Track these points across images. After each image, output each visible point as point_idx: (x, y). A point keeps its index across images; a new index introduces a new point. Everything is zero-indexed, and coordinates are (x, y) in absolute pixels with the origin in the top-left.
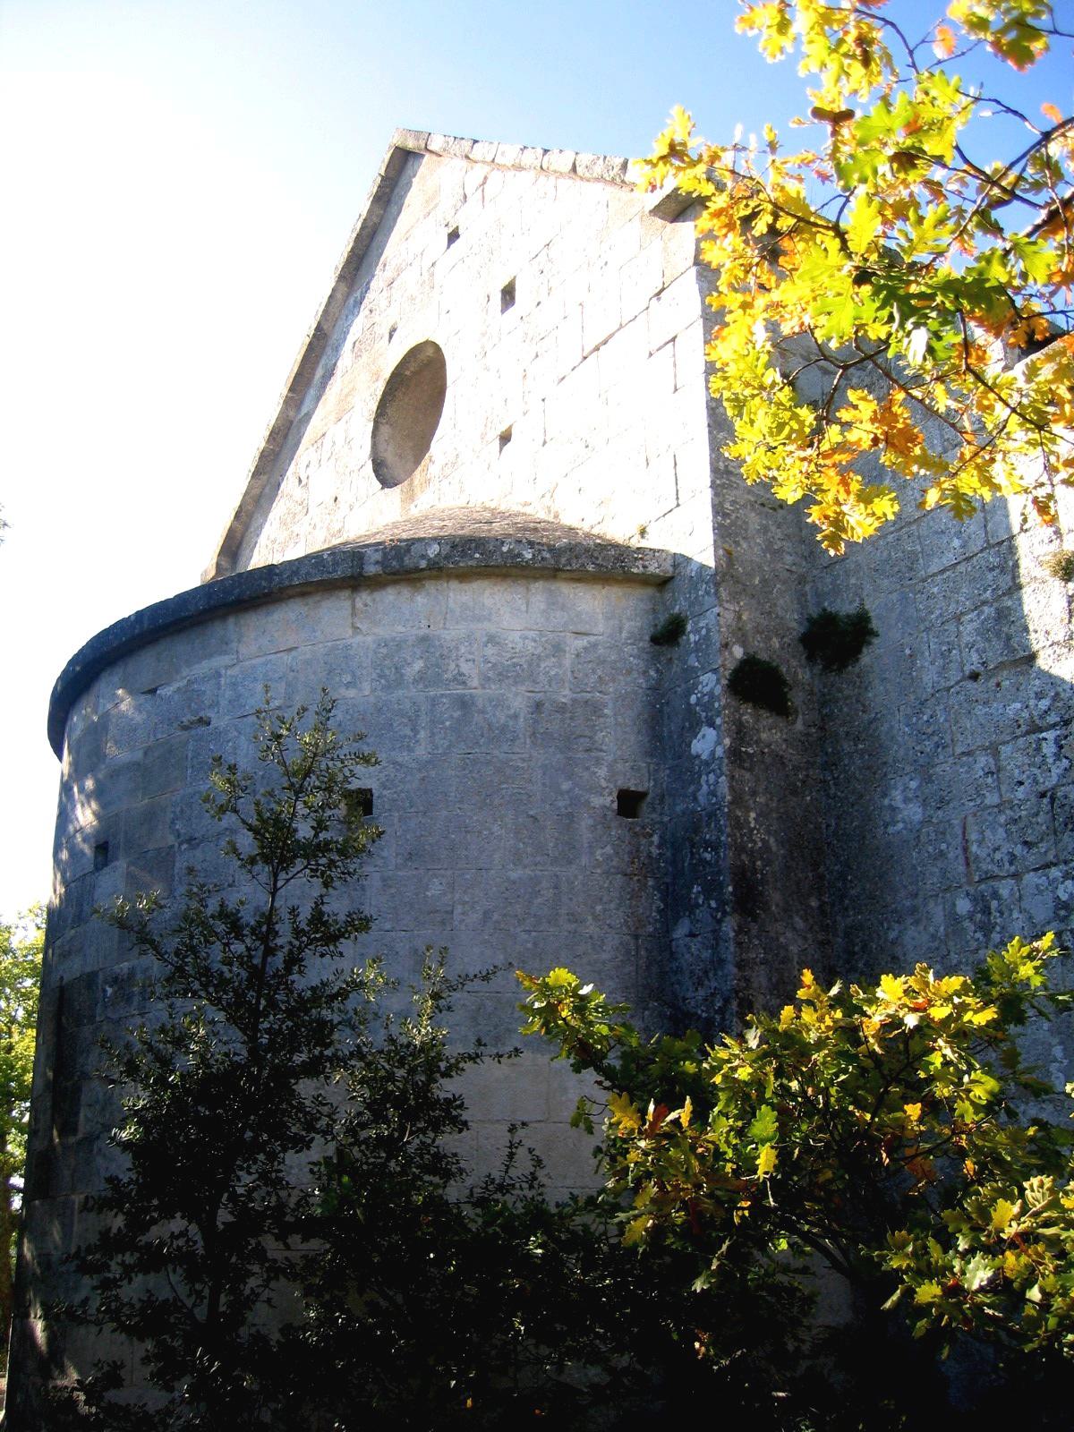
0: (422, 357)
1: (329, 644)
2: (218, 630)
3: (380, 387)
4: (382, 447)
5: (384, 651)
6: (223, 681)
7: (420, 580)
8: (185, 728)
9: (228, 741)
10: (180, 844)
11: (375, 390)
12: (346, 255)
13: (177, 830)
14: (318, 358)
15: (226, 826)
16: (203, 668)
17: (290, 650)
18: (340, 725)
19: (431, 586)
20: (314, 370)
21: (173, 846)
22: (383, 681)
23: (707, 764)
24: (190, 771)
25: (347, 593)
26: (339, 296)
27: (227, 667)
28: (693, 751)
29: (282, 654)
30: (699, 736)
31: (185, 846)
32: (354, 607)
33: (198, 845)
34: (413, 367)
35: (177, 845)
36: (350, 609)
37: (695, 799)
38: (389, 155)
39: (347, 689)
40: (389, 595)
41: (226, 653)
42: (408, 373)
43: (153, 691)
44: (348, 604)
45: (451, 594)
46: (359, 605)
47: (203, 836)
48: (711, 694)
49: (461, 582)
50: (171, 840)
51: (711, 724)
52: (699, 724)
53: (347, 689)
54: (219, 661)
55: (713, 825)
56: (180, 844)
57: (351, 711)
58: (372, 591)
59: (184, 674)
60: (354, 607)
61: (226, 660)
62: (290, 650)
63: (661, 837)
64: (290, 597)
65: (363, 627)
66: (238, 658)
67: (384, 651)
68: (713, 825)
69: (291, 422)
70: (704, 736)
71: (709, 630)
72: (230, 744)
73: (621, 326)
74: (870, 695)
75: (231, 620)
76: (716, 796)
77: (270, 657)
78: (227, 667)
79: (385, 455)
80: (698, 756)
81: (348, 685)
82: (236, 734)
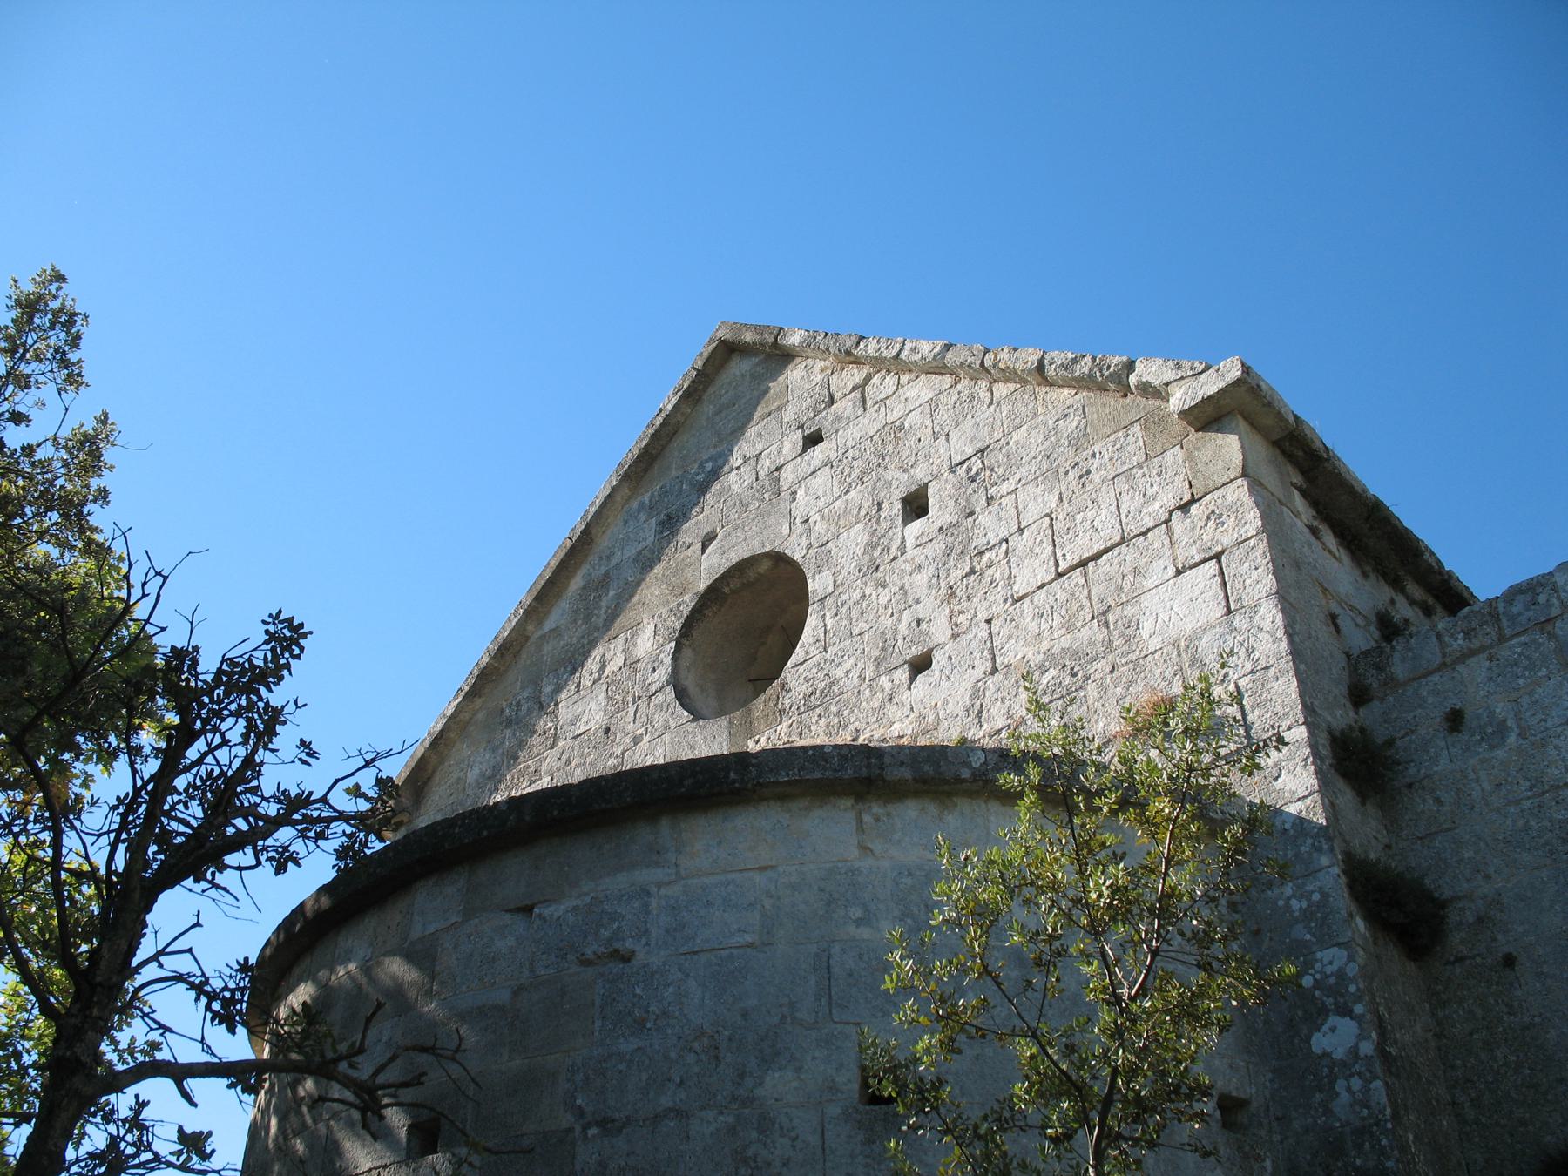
0: (751, 574)
1: (828, 865)
2: (643, 834)
3: (688, 602)
4: (683, 673)
5: (908, 881)
6: (654, 903)
7: (949, 794)
8: (585, 963)
9: (667, 985)
10: (585, 1128)
11: (679, 605)
12: (636, 452)
13: (580, 1107)
14: (578, 566)
15: (670, 1104)
16: (621, 881)
17: (765, 868)
18: (851, 975)
19: (964, 805)
20: (569, 578)
21: (570, 1130)
22: (909, 921)
23: (1343, 1064)
24: (598, 1024)
25: (848, 802)
26: (618, 498)
27: (659, 885)
28: (1316, 1049)
29: (751, 874)
30: (1325, 1028)
31: (593, 1131)
32: (860, 821)
33: (620, 1131)
34: (734, 584)
35: (578, 1128)
36: (854, 823)
37: (1328, 1111)
38: (710, 348)
39: (857, 927)
40: (910, 810)
41: (657, 864)
42: (726, 590)
43: (527, 910)
44: (850, 816)
45: (992, 818)
46: (867, 818)
47: (628, 1117)
48: (1340, 974)
49: (1004, 805)
50: (566, 1120)
51: (1346, 1012)
52: (1324, 1012)
53: (857, 927)
54: (644, 876)
55: (1367, 1145)
56: (585, 1128)
57: (866, 958)
58: (886, 802)
59: (585, 889)
60: (860, 821)
61: (658, 874)
62: (765, 868)
63: (1273, 1162)
64: (762, 799)
65: (877, 846)
66: (678, 873)
67: (908, 881)
68: (1367, 1145)
69: (527, 638)
70: (1333, 1029)
71: (1325, 896)
72: (671, 989)
73: (1123, 541)
74: (1519, 993)
75: (665, 824)
76: (1368, 1107)
77: (733, 876)
78: (659, 885)
79: (686, 683)
80: (1326, 1055)
81: (858, 922)
82: (680, 975)
